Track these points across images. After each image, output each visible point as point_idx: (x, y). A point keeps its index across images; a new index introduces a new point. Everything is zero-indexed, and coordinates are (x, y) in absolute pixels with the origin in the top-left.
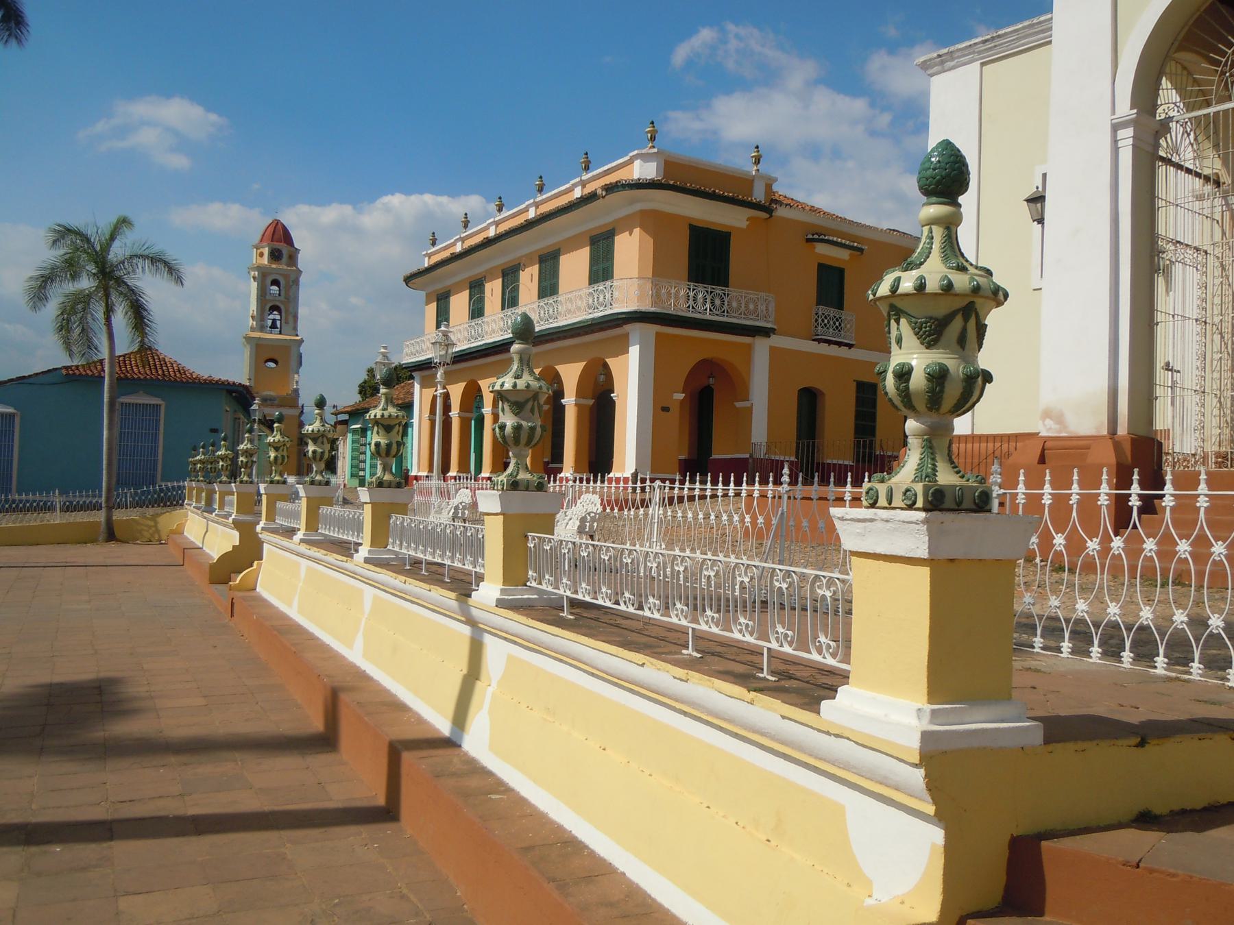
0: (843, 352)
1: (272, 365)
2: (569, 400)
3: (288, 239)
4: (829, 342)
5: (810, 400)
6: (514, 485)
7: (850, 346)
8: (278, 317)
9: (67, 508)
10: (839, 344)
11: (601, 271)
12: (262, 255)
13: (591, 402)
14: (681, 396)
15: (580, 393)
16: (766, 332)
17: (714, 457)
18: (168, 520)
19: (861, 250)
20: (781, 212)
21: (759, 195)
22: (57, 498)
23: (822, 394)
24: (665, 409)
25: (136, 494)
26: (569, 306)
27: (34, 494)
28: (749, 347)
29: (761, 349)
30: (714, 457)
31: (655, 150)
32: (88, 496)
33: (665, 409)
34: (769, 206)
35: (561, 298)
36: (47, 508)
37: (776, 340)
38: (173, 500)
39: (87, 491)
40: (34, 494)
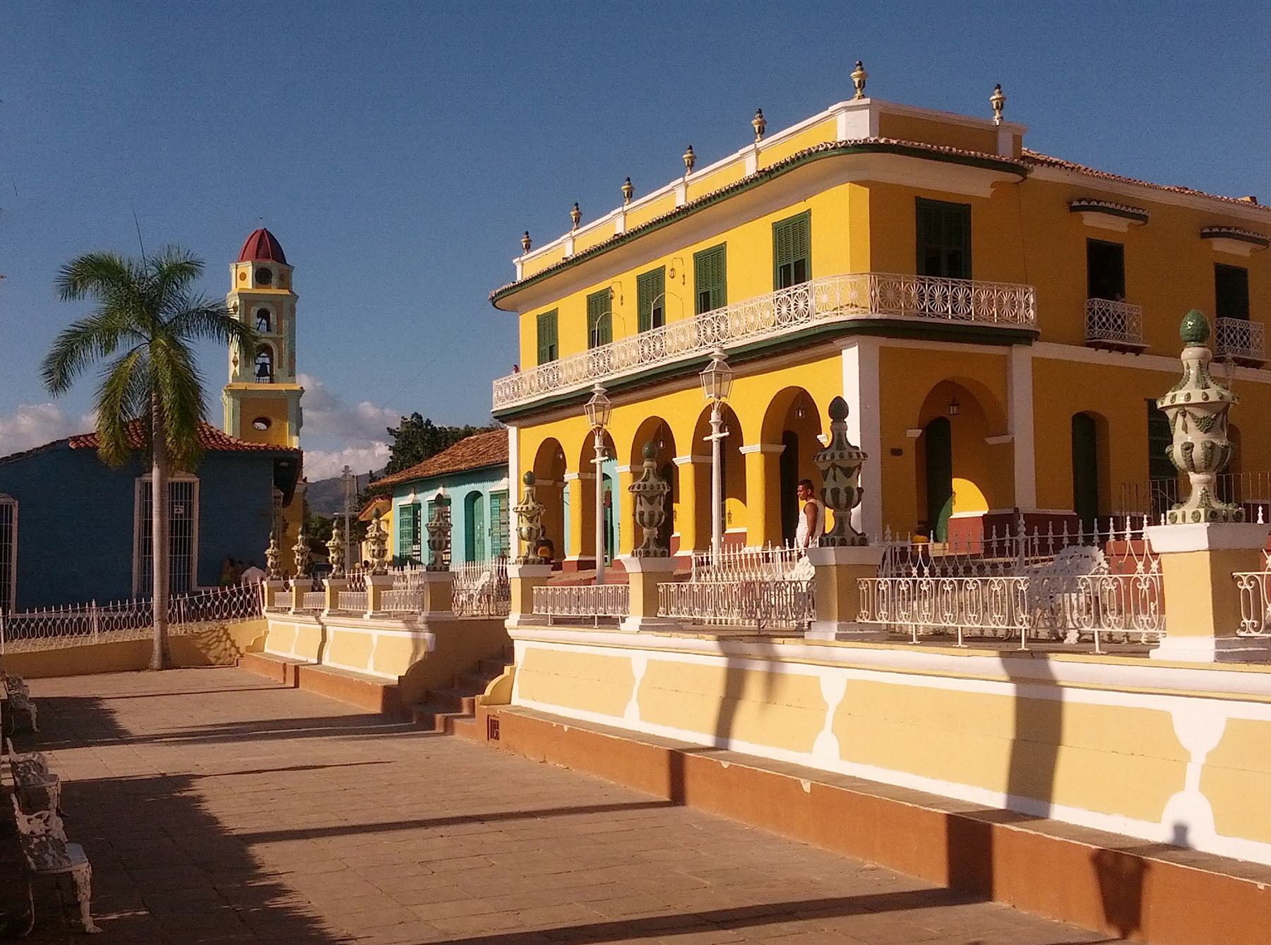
0: (1129, 360)
1: (262, 426)
2: (752, 448)
3: (278, 255)
4: (1110, 347)
5: (1087, 431)
6: (374, 573)
7: (1137, 351)
8: (267, 360)
9: (107, 625)
10: (1123, 349)
11: (792, 269)
12: (243, 277)
13: (782, 448)
14: (916, 433)
15: (766, 438)
16: (1026, 337)
17: (955, 515)
18: (242, 630)
19: (1144, 218)
20: (1038, 173)
21: (1005, 153)
22: (94, 614)
23: (1103, 420)
24: (897, 452)
25: (192, 601)
26: (752, 319)
27: (32, 611)
28: (1005, 362)
29: (1021, 359)
30: (955, 515)
31: (867, 101)
32: (115, 610)
33: (897, 452)
34: (1019, 167)
35: (731, 308)
36: (82, 627)
37: (1040, 349)
38: (249, 608)
39: (123, 602)
40: (32, 611)
